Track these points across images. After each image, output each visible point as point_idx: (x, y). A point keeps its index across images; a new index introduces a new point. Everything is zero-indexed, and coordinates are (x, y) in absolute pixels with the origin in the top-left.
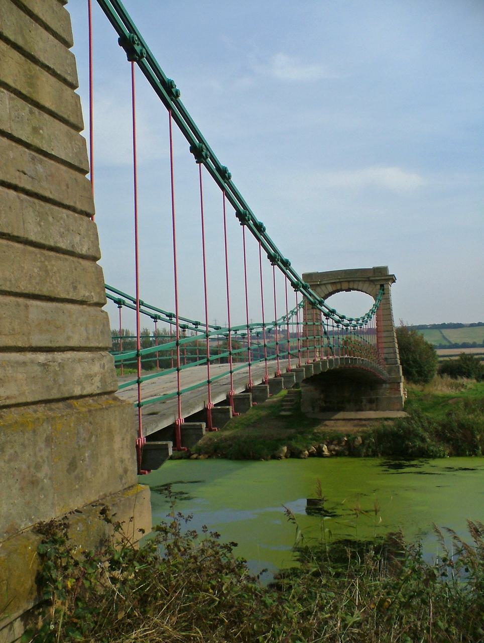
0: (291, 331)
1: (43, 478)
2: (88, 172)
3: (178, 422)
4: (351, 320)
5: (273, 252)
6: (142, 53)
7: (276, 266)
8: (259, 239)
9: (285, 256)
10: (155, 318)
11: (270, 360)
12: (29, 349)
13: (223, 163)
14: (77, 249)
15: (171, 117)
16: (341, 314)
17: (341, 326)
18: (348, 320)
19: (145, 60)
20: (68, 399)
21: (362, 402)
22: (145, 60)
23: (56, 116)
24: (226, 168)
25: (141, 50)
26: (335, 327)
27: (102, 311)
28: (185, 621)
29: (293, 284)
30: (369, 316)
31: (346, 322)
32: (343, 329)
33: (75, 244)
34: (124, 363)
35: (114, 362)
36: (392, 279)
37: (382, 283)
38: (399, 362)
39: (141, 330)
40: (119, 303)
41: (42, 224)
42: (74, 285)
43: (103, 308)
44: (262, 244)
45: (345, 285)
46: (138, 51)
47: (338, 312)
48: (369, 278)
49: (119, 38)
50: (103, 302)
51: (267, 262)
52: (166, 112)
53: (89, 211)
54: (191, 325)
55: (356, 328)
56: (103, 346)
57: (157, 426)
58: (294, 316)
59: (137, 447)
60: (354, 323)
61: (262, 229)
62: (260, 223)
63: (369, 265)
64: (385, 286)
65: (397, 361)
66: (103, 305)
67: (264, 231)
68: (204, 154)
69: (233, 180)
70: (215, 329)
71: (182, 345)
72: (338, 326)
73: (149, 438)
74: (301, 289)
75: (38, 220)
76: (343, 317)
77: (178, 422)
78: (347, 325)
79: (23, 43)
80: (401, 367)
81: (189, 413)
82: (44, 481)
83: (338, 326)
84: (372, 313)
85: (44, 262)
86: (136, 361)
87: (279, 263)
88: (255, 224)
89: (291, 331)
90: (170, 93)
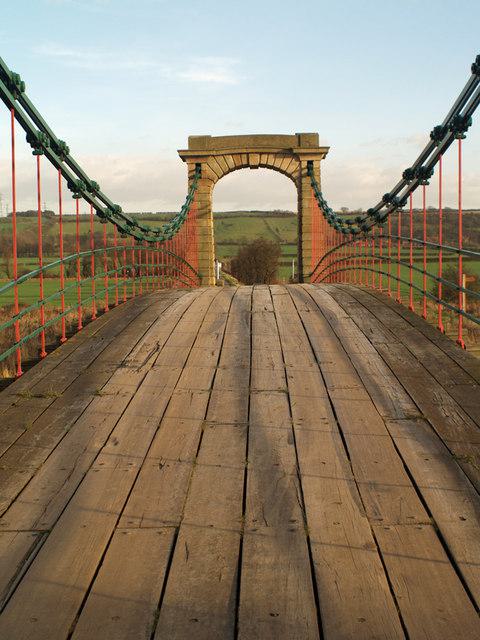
5: (37, 129)
7: (43, 158)
8: (58, 166)
9: (59, 134)
15: (15, 120)
24: (17, 76)
29: (71, 185)
36: (323, 153)
37: (310, 159)
39: (427, 207)
44: (17, 115)
45: (255, 160)
48: (291, 149)
51: (25, 149)
52: (8, 113)
61: (19, 87)
63: (290, 130)
64: (315, 164)
67: (23, 91)
69: (28, 93)
74: (49, 150)
87: (49, 150)
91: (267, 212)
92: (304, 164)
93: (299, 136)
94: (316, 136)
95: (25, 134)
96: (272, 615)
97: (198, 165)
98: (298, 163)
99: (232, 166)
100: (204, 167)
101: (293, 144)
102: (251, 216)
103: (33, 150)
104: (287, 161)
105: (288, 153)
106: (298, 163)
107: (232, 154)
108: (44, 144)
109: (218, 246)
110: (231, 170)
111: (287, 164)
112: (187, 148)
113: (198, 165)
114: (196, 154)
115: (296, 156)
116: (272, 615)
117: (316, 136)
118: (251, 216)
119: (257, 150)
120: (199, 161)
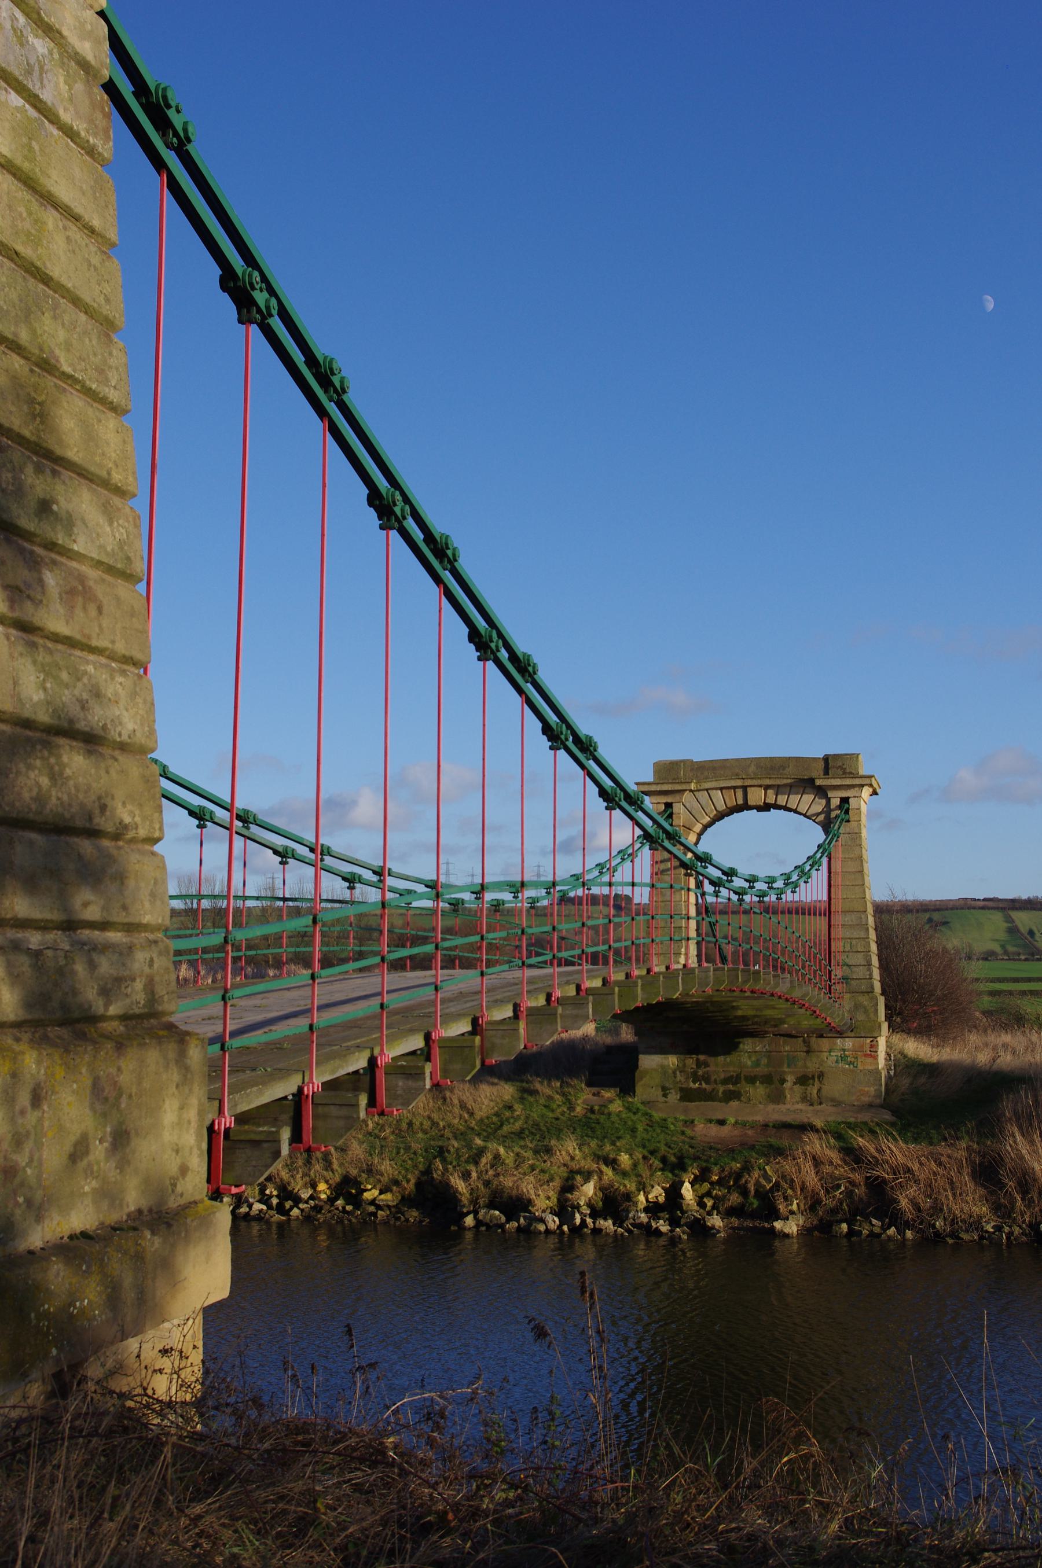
0: (636, 900)
1: (24, 1164)
2: (141, 580)
3: (308, 1090)
4: (752, 880)
6: (268, 308)
7: (490, 664)
8: (582, 766)
9: (584, 729)
10: (284, 855)
11: (531, 966)
12: (12, 922)
13: (439, 526)
14: (113, 733)
16: (727, 864)
17: (724, 892)
18: (746, 880)
19: (276, 324)
20: (78, 1021)
21: (783, 1081)
22: (276, 324)
23: (83, 472)
25: (267, 301)
26: (710, 895)
27: (153, 854)
28: (270, 1433)
29: (603, 793)
30: (803, 873)
31: (738, 883)
32: (729, 899)
33: (108, 722)
34: (206, 956)
35: (172, 953)
37: (844, 794)
38: (878, 987)
40: (200, 816)
41: (48, 685)
42: (102, 801)
43: (157, 848)
46: (262, 305)
47: (716, 858)
48: (812, 781)
49: (221, 276)
50: (157, 835)
53: (138, 656)
54: (368, 875)
55: (766, 899)
56: (154, 923)
57: (261, 1093)
58: (628, 864)
59: (211, 1130)
60: (760, 886)
62: (524, 654)
65: (872, 987)
66: (157, 840)
68: (397, 510)
70: (427, 886)
71: (237, 947)
72: (716, 894)
73: (242, 1119)
74: (624, 804)
75: (41, 678)
76: (730, 873)
77: (308, 1090)
78: (740, 893)
79: (57, 487)
80: (882, 1001)
81: (333, 1072)
82: (26, 1172)
83: (716, 894)
84: (812, 866)
85: (47, 759)
86: (223, 955)
88: (514, 657)
89: (636, 900)
90: (325, 381)
91: (1013, 901)
92: (835, 802)
93: (826, 759)
94: (854, 757)
95: (597, 790)
96: (540, 1333)
97: (669, 805)
98: (824, 802)
99: (721, 807)
100: (678, 808)
101: (817, 771)
102: (983, 908)
103: (605, 804)
104: (808, 798)
105: (807, 784)
106: (824, 802)
107: (721, 789)
108: (617, 799)
109: (822, 764)
110: (720, 816)
111: (807, 801)
112: (651, 780)
113: (669, 805)
114: (665, 787)
115: (821, 792)
116: (540, 1333)
117: (854, 757)
118: (983, 908)
119: (759, 782)
120: (669, 799)
